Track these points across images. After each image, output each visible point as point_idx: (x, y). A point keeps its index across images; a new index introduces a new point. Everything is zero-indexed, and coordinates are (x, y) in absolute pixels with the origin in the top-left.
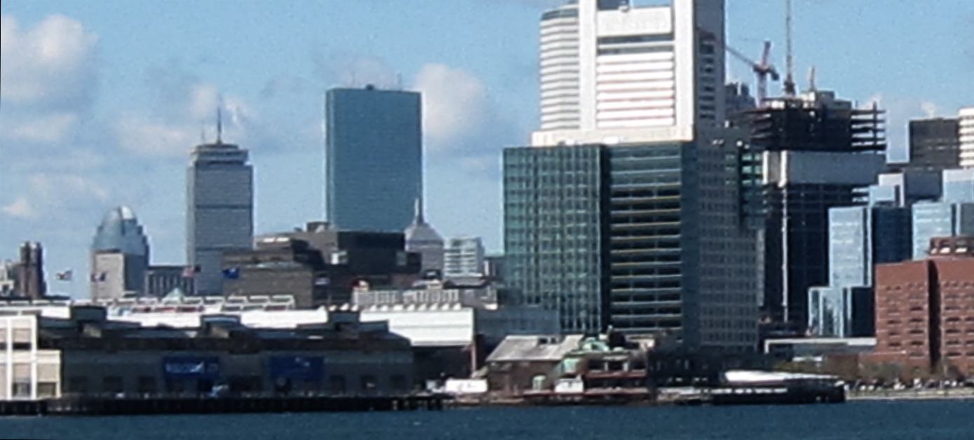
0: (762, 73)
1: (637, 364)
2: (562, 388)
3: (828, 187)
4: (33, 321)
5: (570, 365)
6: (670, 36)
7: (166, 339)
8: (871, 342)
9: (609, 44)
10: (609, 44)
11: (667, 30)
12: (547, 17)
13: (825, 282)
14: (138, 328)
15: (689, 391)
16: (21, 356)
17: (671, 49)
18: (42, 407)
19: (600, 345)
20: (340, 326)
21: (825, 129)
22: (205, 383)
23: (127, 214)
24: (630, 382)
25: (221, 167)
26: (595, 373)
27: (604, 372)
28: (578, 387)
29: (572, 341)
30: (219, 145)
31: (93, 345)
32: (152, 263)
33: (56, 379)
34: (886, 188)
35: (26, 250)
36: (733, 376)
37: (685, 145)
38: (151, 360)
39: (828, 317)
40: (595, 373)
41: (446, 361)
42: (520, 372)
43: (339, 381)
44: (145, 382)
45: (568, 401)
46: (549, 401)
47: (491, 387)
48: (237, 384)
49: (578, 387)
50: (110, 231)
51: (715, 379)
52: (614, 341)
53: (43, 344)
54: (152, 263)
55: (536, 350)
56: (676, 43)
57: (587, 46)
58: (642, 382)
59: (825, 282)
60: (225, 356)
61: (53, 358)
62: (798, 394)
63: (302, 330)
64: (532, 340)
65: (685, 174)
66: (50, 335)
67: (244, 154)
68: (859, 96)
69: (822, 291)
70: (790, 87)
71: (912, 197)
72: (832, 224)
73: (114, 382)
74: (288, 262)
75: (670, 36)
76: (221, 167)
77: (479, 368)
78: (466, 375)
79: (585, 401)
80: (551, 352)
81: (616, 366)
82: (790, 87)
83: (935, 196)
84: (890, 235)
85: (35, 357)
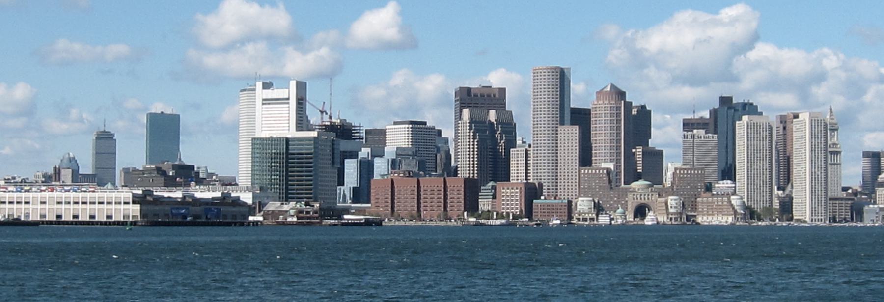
0: (322, 112)
1: (316, 212)
2: (289, 220)
3: (350, 152)
4: (130, 195)
5: (292, 212)
6: (288, 99)
7: (171, 201)
8: (369, 205)
9: (266, 101)
10: (266, 101)
11: (287, 96)
12: (242, 91)
13: (343, 185)
14: (163, 197)
15: (333, 222)
16: (127, 206)
17: (288, 103)
18: (134, 224)
19: (302, 205)
20: (225, 197)
21: (344, 131)
22: (185, 217)
23: (71, 155)
24: (314, 218)
25: (105, 141)
26: (301, 215)
27: (304, 215)
28: (295, 219)
29: (292, 204)
30: (104, 131)
31: (150, 203)
32: (80, 172)
33: (139, 214)
34: (364, 153)
35: (55, 168)
36: (346, 217)
37: (315, 138)
38: (168, 208)
39: (344, 196)
40: (301, 215)
41: (251, 210)
42: (275, 214)
43: (225, 217)
44: (167, 215)
45: (292, 224)
46: (284, 224)
47: (264, 219)
48: (196, 217)
49: (295, 219)
50: (65, 161)
51: (340, 218)
52: (307, 204)
53: (134, 203)
54: (80, 172)
55: (280, 207)
56: (290, 101)
57: (259, 102)
58: (317, 218)
59: (343, 185)
60: (191, 208)
61: (138, 207)
62: (368, 223)
63: (213, 199)
64: (279, 204)
65: (315, 148)
66: (136, 200)
67: (113, 135)
68: (353, 120)
69: (342, 188)
70: (330, 117)
71: (373, 156)
72: (346, 165)
73: (156, 215)
74: (155, 174)
75: (288, 99)
76: (105, 141)
77: (260, 211)
78: (254, 215)
79: (297, 224)
80: (286, 207)
81: (308, 212)
82: (330, 117)
83: (381, 156)
84: (367, 168)
85: (131, 206)
